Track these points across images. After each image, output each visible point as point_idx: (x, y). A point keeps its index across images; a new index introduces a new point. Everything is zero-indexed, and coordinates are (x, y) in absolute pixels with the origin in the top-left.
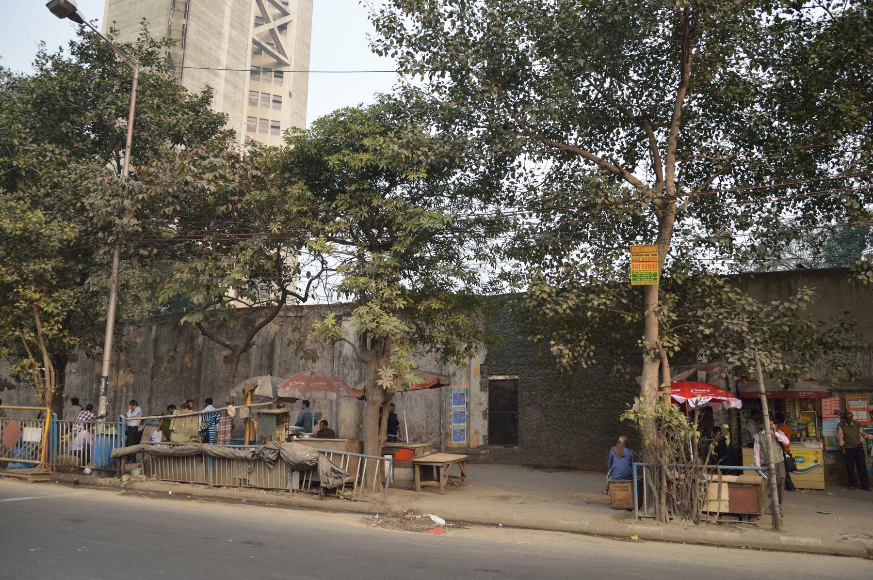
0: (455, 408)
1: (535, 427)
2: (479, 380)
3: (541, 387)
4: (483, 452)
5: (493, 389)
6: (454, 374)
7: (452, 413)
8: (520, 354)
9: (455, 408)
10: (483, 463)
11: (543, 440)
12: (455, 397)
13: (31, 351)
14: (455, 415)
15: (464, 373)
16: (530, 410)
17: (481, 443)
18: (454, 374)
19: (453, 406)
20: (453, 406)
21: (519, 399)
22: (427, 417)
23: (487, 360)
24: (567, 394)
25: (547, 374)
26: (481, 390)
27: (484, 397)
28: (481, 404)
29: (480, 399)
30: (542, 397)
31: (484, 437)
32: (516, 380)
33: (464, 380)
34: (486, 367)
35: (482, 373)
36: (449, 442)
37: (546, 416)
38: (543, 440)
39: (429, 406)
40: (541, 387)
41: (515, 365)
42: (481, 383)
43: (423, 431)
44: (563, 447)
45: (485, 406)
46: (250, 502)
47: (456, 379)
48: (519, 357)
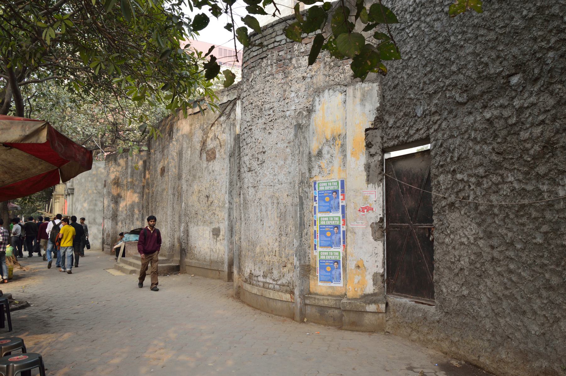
0: (323, 218)
1: (464, 262)
2: (363, 159)
3: (476, 160)
4: (372, 308)
5: (389, 175)
6: (320, 154)
7: (317, 228)
8: (431, 89)
9: (323, 218)
10: (372, 331)
11: (484, 300)
12: (322, 198)
13: (339, 206)
14: (323, 233)
15: (336, 151)
16: (454, 219)
17: (370, 288)
18: (320, 154)
19: (319, 215)
20: (319, 215)
21: (434, 193)
22: (281, 235)
23: (379, 120)
24: (542, 170)
25: (489, 121)
26: (368, 181)
27: (375, 195)
28: (369, 209)
29: (366, 199)
30: (479, 184)
31: (375, 275)
32: (428, 151)
33: (337, 162)
34: (378, 133)
35: (369, 145)
36: (312, 283)
37: (489, 235)
38: (484, 300)
39: (282, 216)
40: (476, 160)
41: (424, 115)
42: (368, 167)
43: (275, 259)
44: (535, 329)
45: (378, 212)
46: (422, 303)
47: (323, 163)
48: (430, 96)
